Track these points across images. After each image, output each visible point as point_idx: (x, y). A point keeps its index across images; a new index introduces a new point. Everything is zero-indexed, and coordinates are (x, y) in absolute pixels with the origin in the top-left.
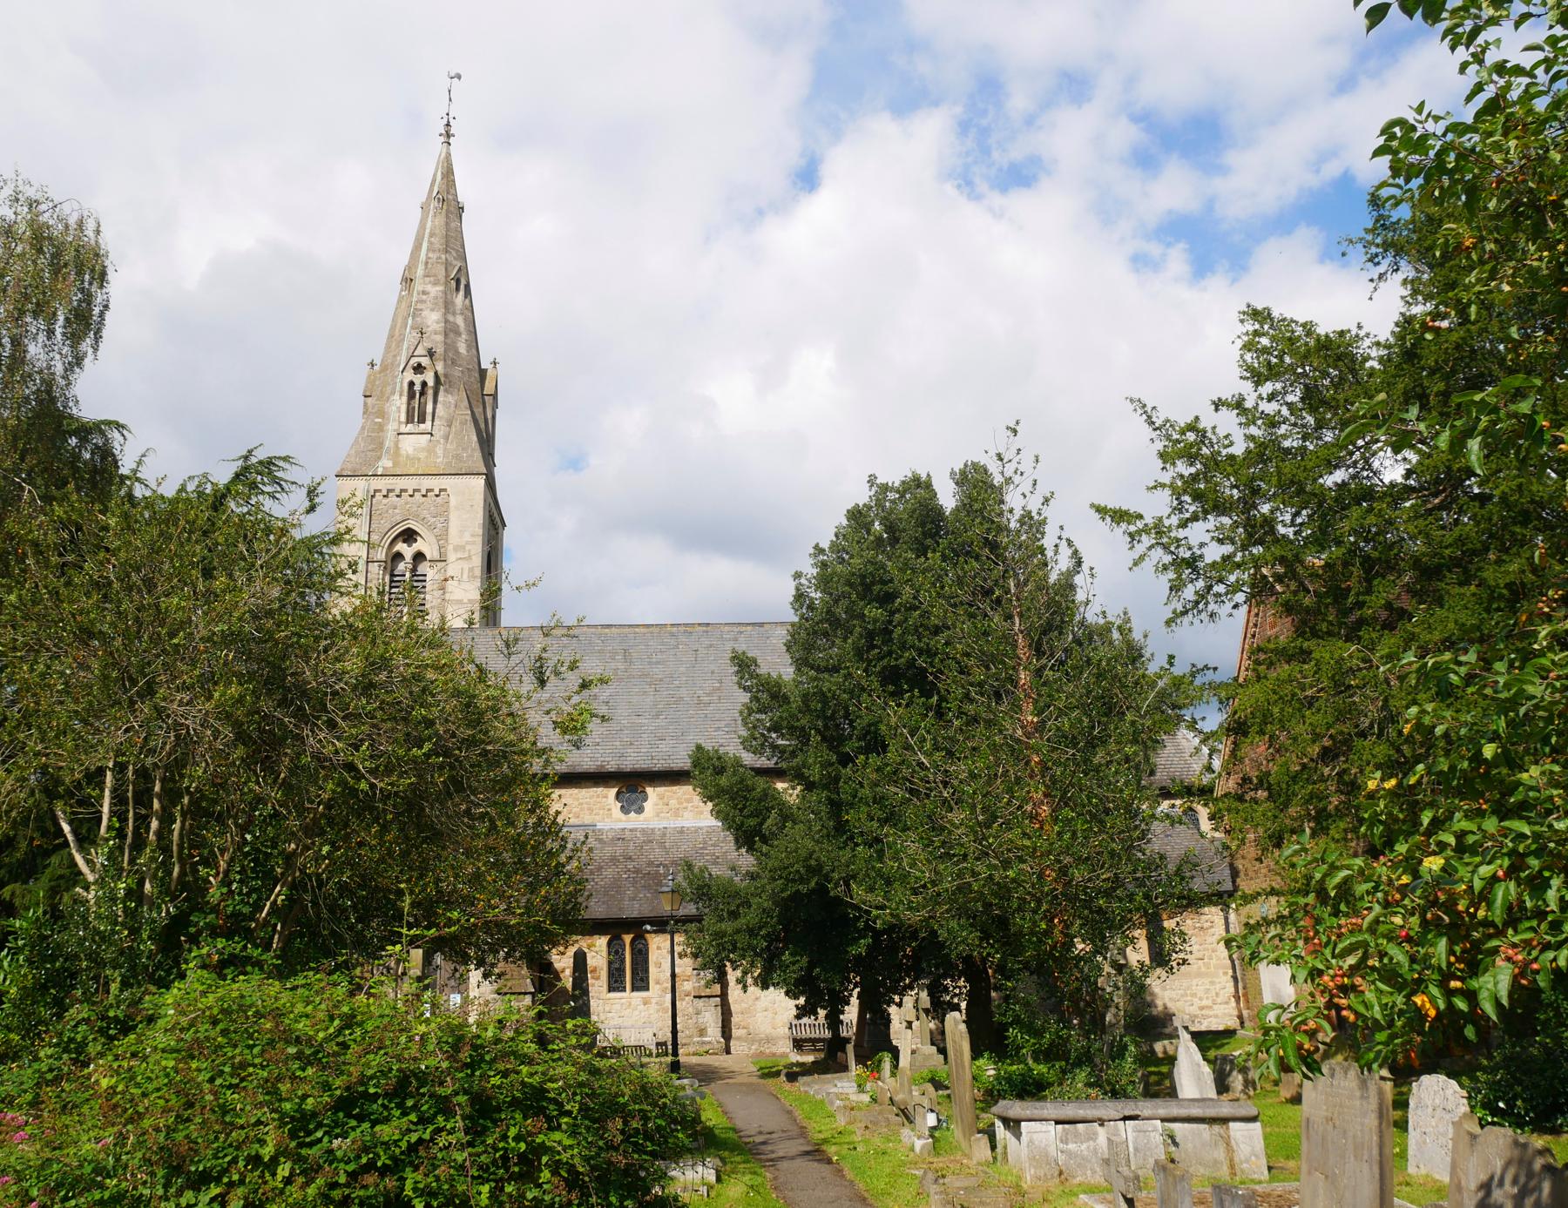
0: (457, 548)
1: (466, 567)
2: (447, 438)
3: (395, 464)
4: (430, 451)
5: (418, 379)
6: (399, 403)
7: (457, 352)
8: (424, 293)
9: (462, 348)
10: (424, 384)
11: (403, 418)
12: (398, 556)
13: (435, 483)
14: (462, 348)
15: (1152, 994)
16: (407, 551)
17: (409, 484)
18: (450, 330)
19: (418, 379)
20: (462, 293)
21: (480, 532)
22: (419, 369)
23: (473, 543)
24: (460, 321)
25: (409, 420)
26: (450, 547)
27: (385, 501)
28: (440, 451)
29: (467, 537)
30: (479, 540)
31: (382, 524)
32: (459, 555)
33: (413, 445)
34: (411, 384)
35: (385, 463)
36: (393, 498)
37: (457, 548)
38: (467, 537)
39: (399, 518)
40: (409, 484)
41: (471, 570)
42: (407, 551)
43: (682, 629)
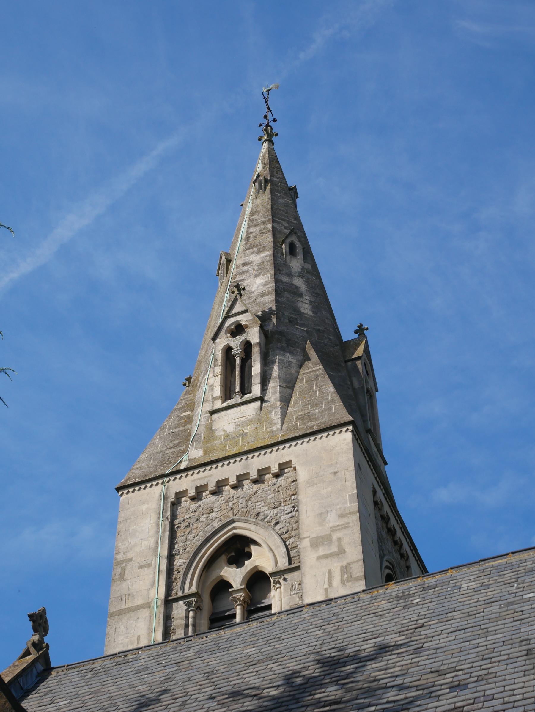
0: (315, 543)
1: (336, 566)
2: (286, 400)
4: (261, 419)
5: (236, 343)
6: (212, 381)
7: (297, 311)
9: (306, 308)
11: (217, 391)
12: (224, 586)
13: (271, 460)
14: (306, 308)
15: (305, 284)
16: (235, 576)
17: (230, 471)
18: (282, 290)
19: (236, 343)
20: (301, 256)
21: (355, 506)
22: (238, 330)
23: (346, 526)
24: (299, 282)
25: (227, 392)
26: (305, 544)
27: (194, 506)
28: (276, 417)
29: (332, 520)
30: (354, 520)
31: (188, 541)
33: (234, 421)
34: (228, 350)
35: (196, 453)
36: (208, 499)
37: (315, 543)
38: (332, 520)
39: (216, 525)
40: (230, 471)
41: (346, 570)
42: (235, 576)
43: (349, 599)
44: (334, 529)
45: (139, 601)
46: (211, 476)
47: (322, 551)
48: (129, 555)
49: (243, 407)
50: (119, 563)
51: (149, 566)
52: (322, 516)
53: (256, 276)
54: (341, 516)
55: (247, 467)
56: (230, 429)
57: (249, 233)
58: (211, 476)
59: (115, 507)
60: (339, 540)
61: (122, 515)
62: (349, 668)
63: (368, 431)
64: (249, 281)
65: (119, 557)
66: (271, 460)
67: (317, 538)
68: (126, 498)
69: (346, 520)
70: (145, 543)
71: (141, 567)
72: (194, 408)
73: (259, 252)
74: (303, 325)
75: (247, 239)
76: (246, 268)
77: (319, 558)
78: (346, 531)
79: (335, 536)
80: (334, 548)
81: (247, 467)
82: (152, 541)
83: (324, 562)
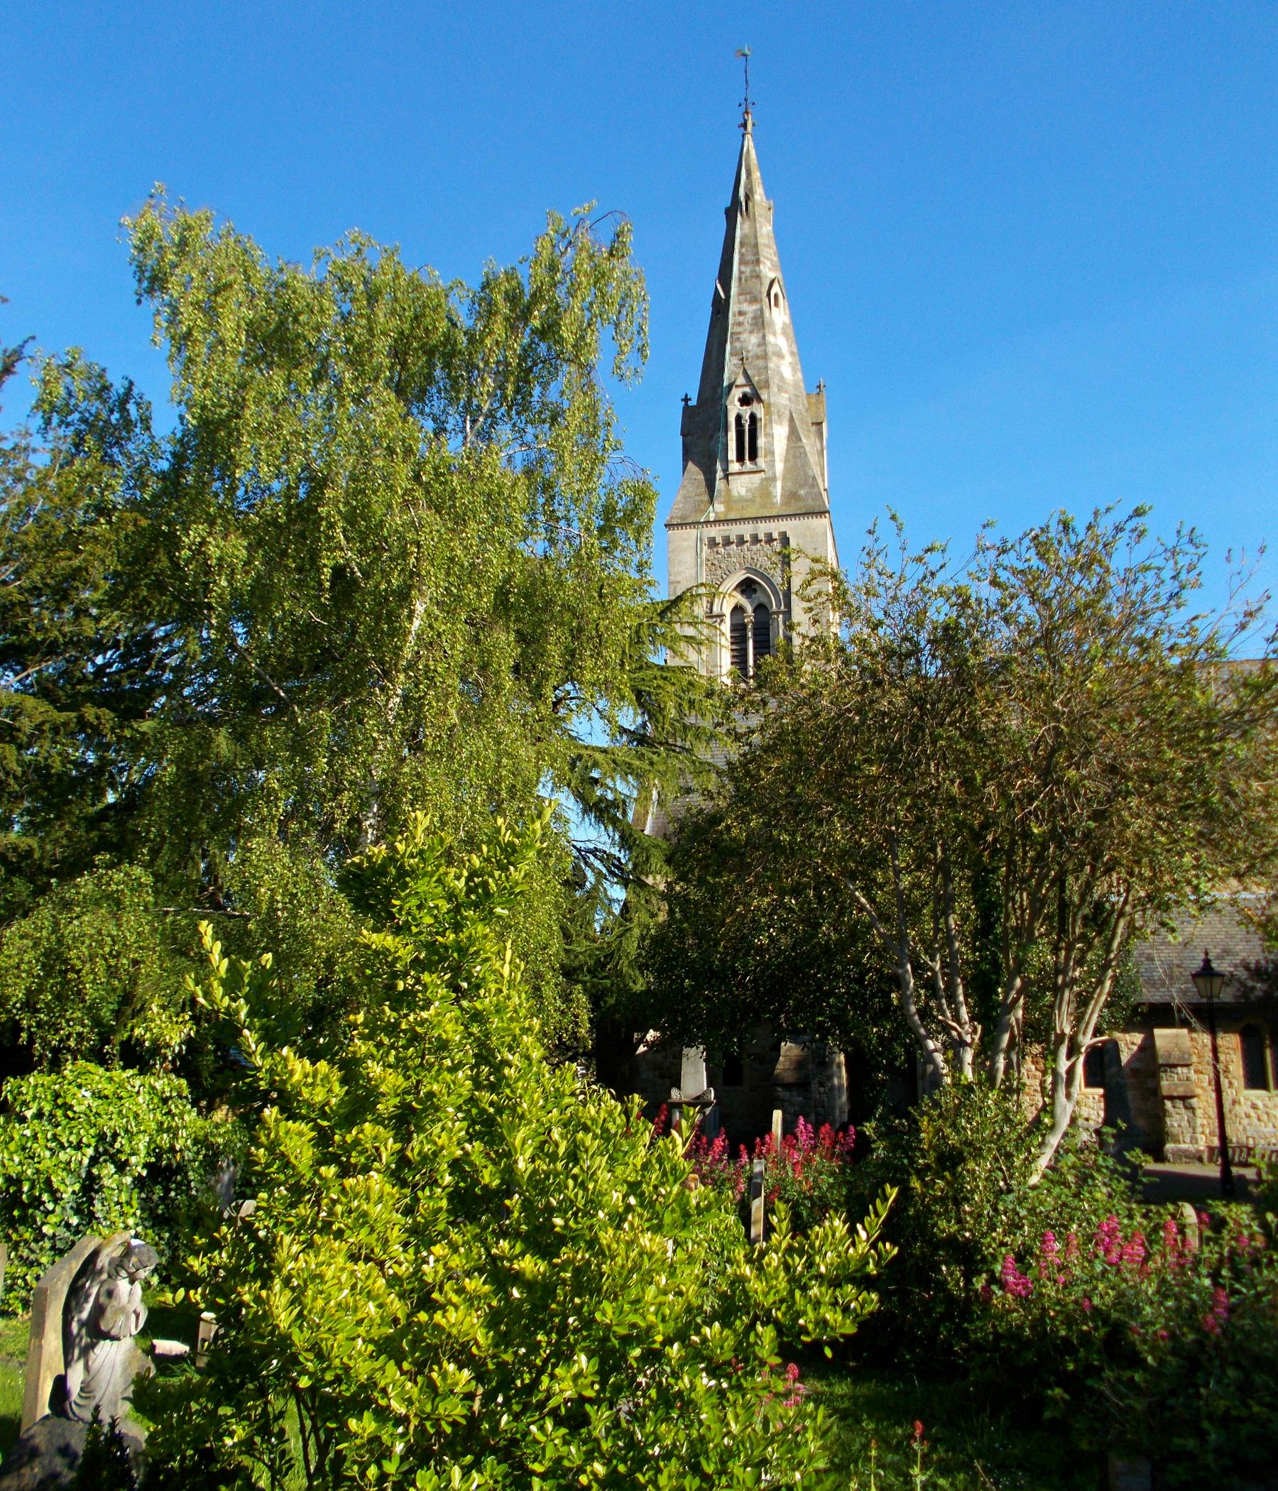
3: (729, 509)
8: (741, 313)
10: (753, 418)
13: (775, 528)
17: (746, 530)
40: (746, 530)
46: (734, 531)
53: (751, 332)
57: (741, 272)
58: (734, 531)
66: (775, 528)
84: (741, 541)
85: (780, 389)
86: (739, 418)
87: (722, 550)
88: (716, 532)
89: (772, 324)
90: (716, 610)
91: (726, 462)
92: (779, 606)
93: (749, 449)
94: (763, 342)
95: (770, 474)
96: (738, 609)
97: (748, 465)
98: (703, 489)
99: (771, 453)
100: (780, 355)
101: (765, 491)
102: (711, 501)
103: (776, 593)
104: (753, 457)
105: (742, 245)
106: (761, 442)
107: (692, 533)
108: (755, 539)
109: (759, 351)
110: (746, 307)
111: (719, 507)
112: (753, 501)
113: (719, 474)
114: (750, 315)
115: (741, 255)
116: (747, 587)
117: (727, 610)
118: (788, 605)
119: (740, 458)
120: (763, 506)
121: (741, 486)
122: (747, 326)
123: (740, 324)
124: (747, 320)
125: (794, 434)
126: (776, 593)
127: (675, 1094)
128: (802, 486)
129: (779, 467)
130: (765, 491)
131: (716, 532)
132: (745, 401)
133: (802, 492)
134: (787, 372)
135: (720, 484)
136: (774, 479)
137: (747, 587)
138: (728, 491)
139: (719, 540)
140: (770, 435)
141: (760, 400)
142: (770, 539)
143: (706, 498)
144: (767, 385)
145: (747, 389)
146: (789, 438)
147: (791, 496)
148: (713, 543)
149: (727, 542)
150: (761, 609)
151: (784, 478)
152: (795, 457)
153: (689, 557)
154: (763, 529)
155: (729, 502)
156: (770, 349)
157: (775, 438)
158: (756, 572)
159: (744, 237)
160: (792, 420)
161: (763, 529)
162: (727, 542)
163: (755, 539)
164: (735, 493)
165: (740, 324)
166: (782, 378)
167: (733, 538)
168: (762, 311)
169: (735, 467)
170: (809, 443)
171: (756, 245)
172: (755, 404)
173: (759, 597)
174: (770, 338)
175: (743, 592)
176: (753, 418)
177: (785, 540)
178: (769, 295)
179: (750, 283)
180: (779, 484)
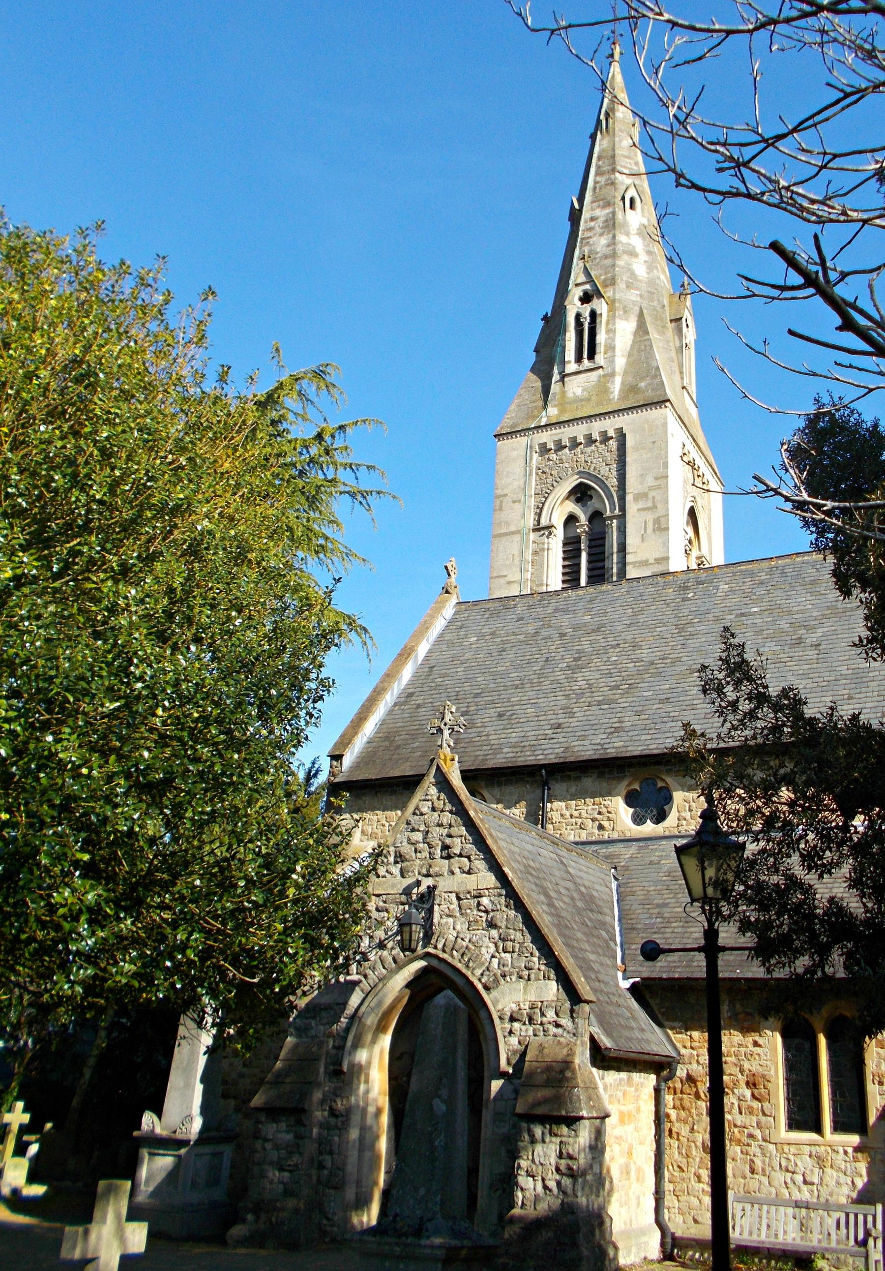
3: (562, 411)
8: (592, 219)
10: (593, 315)
13: (610, 425)
17: (579, 431)
32: (641, 505)
37: (637, 498)
40: (579, 431)
44: (651, 488)
45: (513, 528)
46: (565, 434)
47: (641, 505)
48: (506, 491)
49: (589, 374)
50: (498, 497)
51: (519, 501)
52: (642, 476)
53: (601, 235)
54: (656, 478)
55: (589, 428)
56: (579, 392)
57: (596, 183)
58: (565, 434)
59: (495, 452)
60: (654, 497)
61: (499, 458)
62: (583, 889)
63: (684, 388)
64: (594, 239)
65: (499, 492)
66: (610, 425)
67: (639, 494)
68: (504, 445)
69: (659, 482)
70: (516, 483)
71: (514, 502)
72: (803, 861)
73: (604, 207)
74: (637, 289)
75: (595, 189)
76: (592, 224)
77: (639, 510)
78: (658, 491)
79: (651, 494)
80: (649, 504)
81: (589, 428)
82: (522, 481)
83: (643, 513)
84: (575, 444)
85: (629, 286)
86: (578, 316)
87: (553, 456)
88: (547, 437)
89: (625, 224)
90: (544, 522)
91: (563, 363)
92: (612, 510)
93: (589, 348)
94: (613, 242)
95: (608, 370)
96: (571, 519)
97: (586, 363)
98: (539, 395)
99: (611, 348)
100: (633, 254)
101: (602, 389)
102: (545, 407)
103: (610, 496)
104: (592, 356)
105: (599, 158)
106: (601, 338)
107: (522, 441)
108: (590, 441)
109: (608, 251)
110: (598, 212)
111: (553, 412)
112: (588, 400)
113: (556, 377)
114: (602, 219)
115: (598, 167)
116: (581, 494)
117: (558, 521)
118: (623, 509)
119: (579, 359)
120: (599, 403)
121: (576, 387)
122: (598, 230)
123: (590, 229)
124: (597, 225)
125: (642, 328)
126: (610, 496)
127: (148, 1120)
128: (642, 379)
129: (620, 362)
130: (602, 389)
131: (547, 437)
132: (586, 298)
133: (642, 384)
134: (640, 268)
135: (555, 388)
136: (613, 375)
137: (581, 494)
138: (563, 393)
139: (551, 445)
140: (611, 331)
141: (600, 295)
142: (605, 438)
143: (541, 403)
144: (612, 282)
145: (587, 287)
146: (636, 334)
147: (630, 389)
148: (544, 450)
149: (560, 447)
150: (596, 517)
151: (625, 373)
152: (639, 351)
153: (517, 467)
154: (596, 428)
155: (562, 405)
156: (620, 248)
157: (618, 336)
158: (589, 476)
159: (602, 151)
160: (641, 315)
161: (596, 428)
162: (560, 447)
163: (590, 441)
164: (570, 394)
165: (590, 229)
166: (633, 274)
167: (566, 442)
168: (614, 213)
169: (571, 367)
170: (661, 344)
171: (613, 157)
172: (595, 300)
173: (594, 504)
174: (622, 238)
175: (578, 501)
176: (593, 315)
177: (621, 437)
178: (623, 198)
179: (604, 191)
180: (618, 380)
